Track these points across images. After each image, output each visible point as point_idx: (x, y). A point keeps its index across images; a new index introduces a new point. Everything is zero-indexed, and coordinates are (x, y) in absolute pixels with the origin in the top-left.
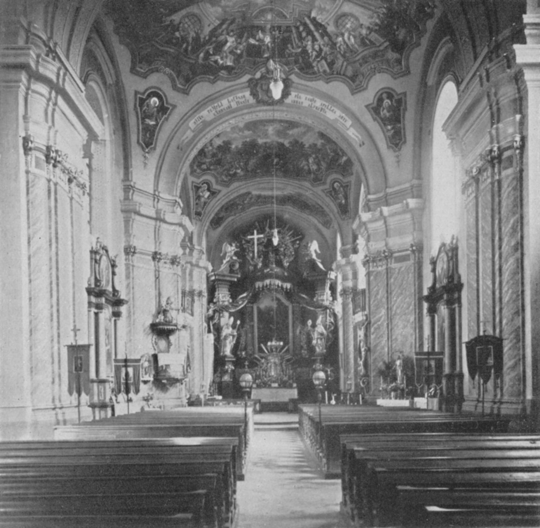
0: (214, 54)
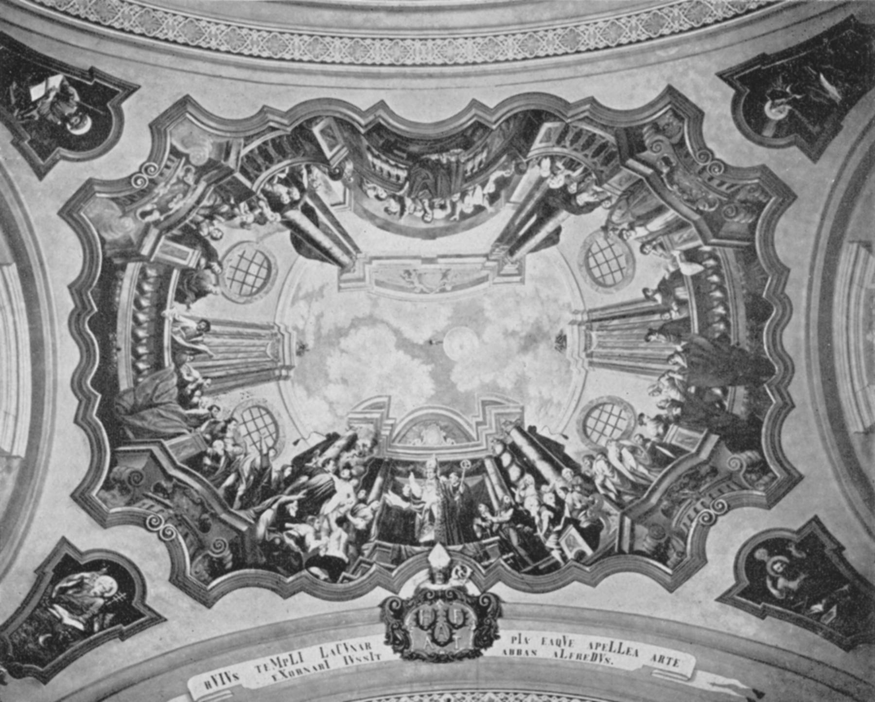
0: (300, 518)
